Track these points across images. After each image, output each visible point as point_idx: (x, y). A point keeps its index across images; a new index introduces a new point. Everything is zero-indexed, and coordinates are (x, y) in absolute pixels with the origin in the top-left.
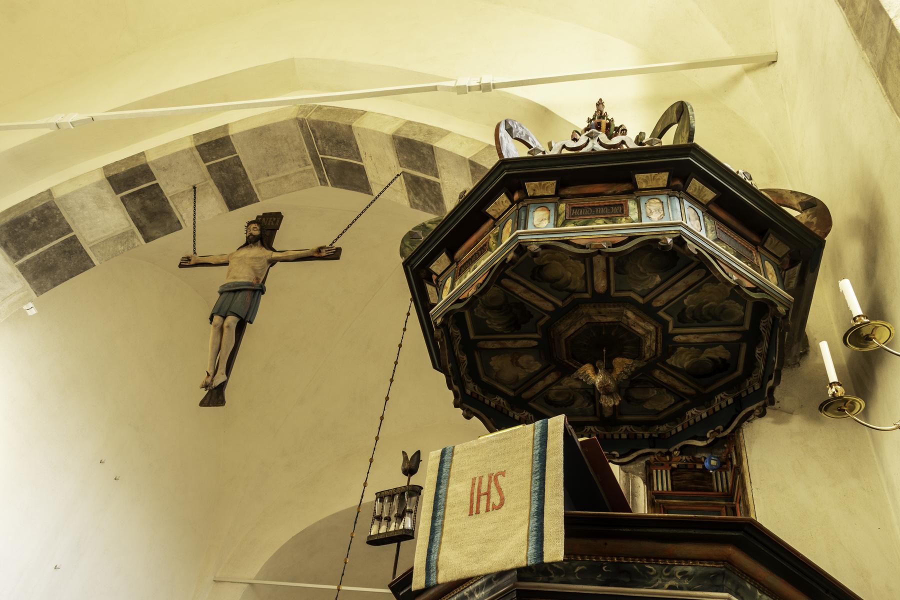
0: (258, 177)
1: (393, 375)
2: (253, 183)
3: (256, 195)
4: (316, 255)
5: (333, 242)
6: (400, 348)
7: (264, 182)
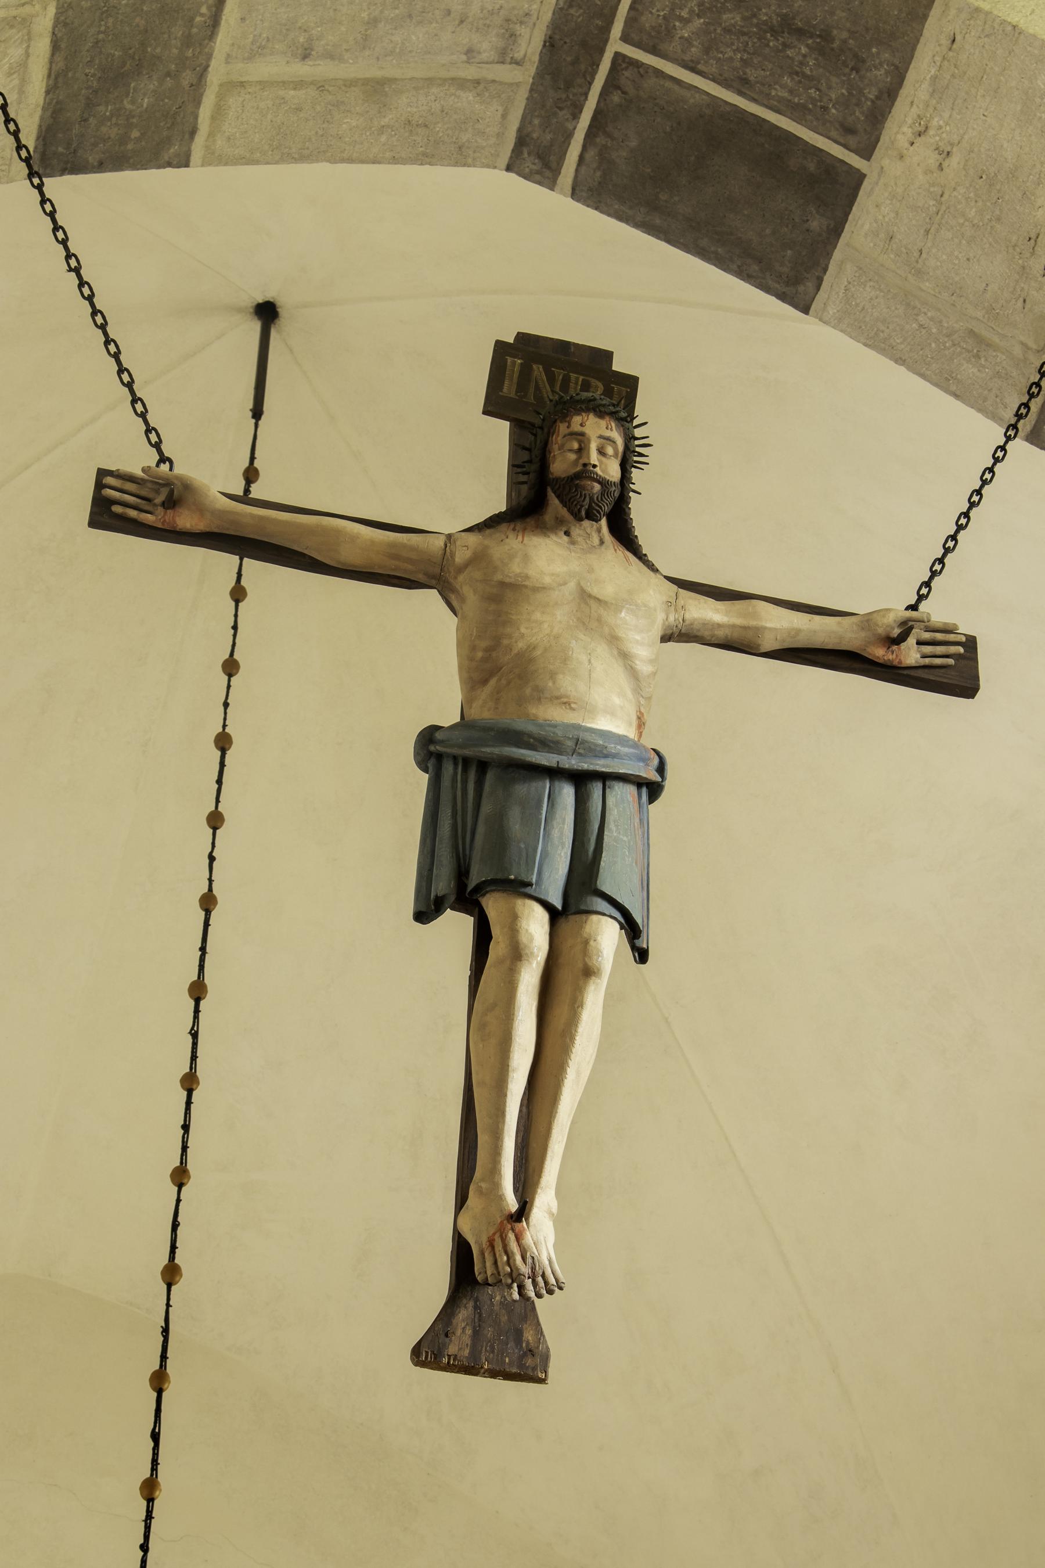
0: (257, 51)
1: (185, 1148)
2: (217, 73)
3: (193, 132)
4: (879, 653)
5: (921, 598)
6: (197, 1001)
7: (263, 84)
